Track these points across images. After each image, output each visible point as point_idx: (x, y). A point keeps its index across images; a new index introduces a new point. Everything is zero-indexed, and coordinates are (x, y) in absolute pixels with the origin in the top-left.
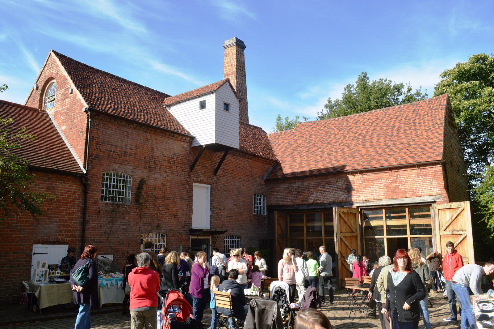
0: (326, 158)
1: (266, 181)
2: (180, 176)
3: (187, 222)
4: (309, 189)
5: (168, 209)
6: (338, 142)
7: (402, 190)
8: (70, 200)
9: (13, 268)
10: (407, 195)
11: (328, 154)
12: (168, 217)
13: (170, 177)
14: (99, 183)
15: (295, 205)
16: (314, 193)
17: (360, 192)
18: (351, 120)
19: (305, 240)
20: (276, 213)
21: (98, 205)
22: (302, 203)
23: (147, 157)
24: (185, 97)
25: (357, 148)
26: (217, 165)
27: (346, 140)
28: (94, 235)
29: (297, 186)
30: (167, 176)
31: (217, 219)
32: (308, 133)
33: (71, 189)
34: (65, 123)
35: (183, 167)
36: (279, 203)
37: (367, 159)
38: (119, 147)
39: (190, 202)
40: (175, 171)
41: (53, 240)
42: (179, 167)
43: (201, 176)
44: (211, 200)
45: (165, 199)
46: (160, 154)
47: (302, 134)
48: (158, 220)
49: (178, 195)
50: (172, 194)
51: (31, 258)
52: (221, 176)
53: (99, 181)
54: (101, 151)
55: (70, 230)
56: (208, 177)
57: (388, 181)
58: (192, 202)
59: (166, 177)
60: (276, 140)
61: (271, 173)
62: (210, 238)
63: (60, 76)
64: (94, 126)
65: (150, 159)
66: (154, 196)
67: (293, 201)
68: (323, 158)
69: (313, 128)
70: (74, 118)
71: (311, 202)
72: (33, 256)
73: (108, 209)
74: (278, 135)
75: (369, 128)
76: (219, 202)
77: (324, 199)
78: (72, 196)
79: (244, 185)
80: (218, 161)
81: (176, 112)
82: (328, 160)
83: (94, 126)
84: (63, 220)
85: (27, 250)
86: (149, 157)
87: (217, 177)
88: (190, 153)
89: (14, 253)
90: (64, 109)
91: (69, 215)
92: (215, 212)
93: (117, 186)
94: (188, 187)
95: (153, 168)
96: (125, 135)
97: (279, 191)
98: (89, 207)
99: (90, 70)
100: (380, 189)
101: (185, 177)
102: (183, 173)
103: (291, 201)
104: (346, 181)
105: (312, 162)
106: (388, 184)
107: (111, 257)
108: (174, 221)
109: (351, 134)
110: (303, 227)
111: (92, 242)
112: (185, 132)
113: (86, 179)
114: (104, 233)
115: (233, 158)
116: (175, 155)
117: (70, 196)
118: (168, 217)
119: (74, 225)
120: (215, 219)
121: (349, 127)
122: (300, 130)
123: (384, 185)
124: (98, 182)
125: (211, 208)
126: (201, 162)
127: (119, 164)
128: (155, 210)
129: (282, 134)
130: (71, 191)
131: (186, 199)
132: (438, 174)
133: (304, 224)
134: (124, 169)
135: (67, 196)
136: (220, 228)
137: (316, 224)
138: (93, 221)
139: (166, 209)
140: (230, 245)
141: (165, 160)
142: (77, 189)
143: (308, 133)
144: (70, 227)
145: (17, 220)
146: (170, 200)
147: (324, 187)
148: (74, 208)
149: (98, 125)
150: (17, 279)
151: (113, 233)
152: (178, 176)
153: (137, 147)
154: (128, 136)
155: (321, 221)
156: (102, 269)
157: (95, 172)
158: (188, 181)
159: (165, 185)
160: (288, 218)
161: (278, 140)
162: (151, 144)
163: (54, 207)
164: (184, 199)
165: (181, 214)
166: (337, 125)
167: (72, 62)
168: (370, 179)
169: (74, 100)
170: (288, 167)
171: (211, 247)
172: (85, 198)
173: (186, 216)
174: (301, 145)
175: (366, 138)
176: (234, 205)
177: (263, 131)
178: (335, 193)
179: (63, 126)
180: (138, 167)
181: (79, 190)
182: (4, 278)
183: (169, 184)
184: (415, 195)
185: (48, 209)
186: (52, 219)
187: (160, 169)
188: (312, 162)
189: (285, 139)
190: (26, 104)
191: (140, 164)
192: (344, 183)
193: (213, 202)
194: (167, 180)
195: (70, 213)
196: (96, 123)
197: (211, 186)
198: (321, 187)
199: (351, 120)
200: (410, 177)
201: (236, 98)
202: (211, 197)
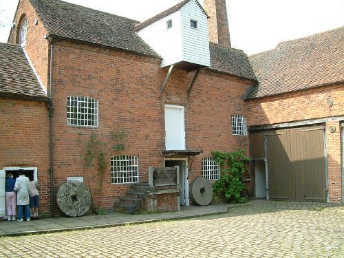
1: (245, 101)
62: (186, 159)
81: (144, 35)
190: (196, 76)
197: (185, 107)
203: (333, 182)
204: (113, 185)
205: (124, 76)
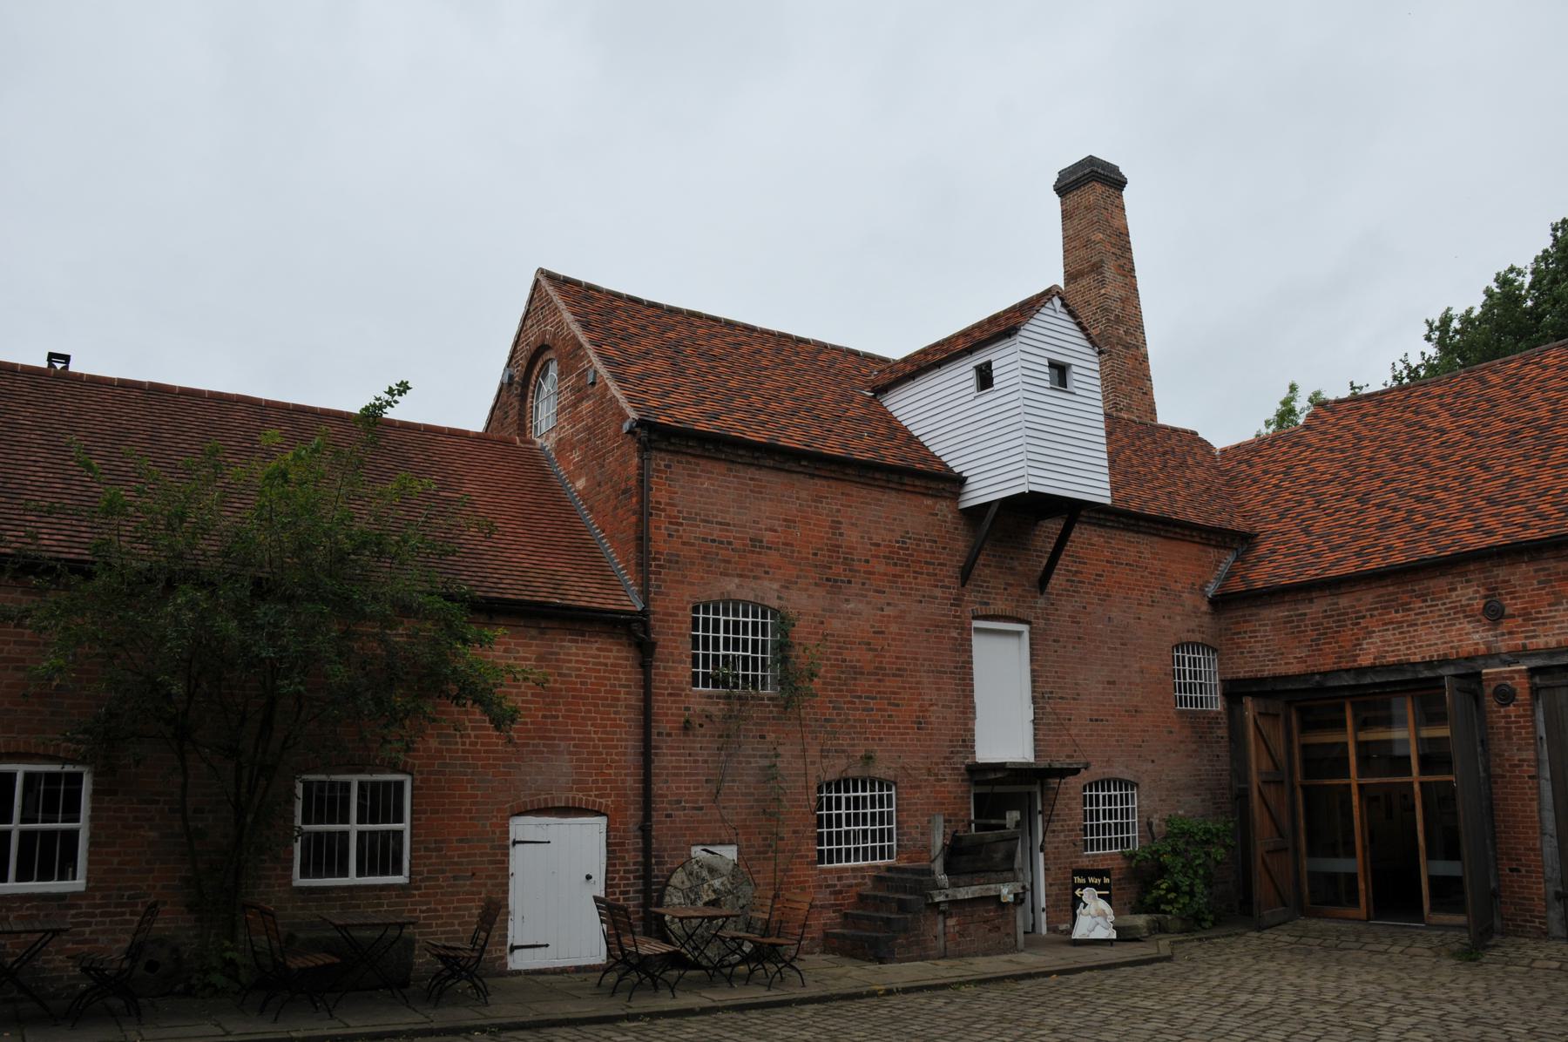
0: (1411, 512)
1: (1214, 602)
2: (930, 602)
4: (1357, 618)
5: (898, 705)
6: (1451, 455)
8: (603, 689)
9: (461, 882)
11: (1418, 499)
12: (899, 728)
13: (896, 605)
14: (684, 635)
15: (1313, 674)
16: (1374, 632)
17: (1537, 619)
18: (1494, 379)
19: (1355, 790)
20: (1248, 702)
21: (684, 702)
22: (1336, 667)
23: (822, 550)
24: (930, 357)
25: (1519, 471)
26: (1045, 562)
27: (1480, 448)
28: (677, 788)
29: (1317, 612)
30: (889, 604)
31: (1055, 730)
32: (1348, 436)
33: (605, 657)
34: (583, 471)
35: (936, 575)
36: (1259, 671)
37: (1553, 504)
39: (964, 679)
40: (911, 589)
41: (563, 805)
42: (922, 573)
43: (994, 599)
44: (1033, 671)
45: (884, 675)
46: (862, 537)
47: (1331, 441)
48: (867, 739)
49: (925, 660)
50: (905, 658)
51: (507, 855)
52: (1061, 595)
53: (683, 631)
54: (684, 543)
55: (610, 775)
56: (1018, 601)
58: (972, 679)
59: (886, 608)
60: (1244, 467)
61: (1231, 574)
63: (564, 339)
64: (659, 471)
65: (829, 556)
66: (852, 667)
67: (1306, 662)
68: (1402, 514)
69: (1364, 416)
70: (604, 455)
71: (1365, 660)
72: (512, 851)
73: (713, 710)
74: (1252, 451)
75: (1559, 400)
76: (1058, 677)
78: (609, 679)
79: (1139, 618)
80: (1049, 548)
82: (1419, 519)
83: (659, 471)
84: (588, 746)
85: (494, 833)
86: (829, 550)
87: (1048, 599)
88: (956, 529)
89: (461, 841)
90: (578, 432)
91: (603, 733)
92: (1049, 710)
93: (736, 641)
94: (955, 635)
95: (842, 581)
96: (751, 491)
97: (1259, 631)
98: (658, 708)
99: (648, 312)
101: (947, 604)
102: (938, 592)
103: (1301, 660)
104: (1483, 584)
105: (1365, 527)
107: (730, 853)
108: (919, 740)
109: (1499, 425)
110: (1346, 744)
111: (672, 810)
112: (937, 466)
113: (646, 627)
114: (707, 781)
115: (1099, 536)
116: (910, 538)
117: (602, 678)
119: (620, 761)
120: (1050, 730)
121: (1488, 401)
122: (1322, 428)
124: (680, 634)
125: (1034, 698)
127: (741, 576)
128: (855, 709)
129: (1265, 446)
130: (606, 665)
131: (951, 673)
133: (1349, 737)
134: (753, 589)
135: (595, 677)
136: (1068, 756)
137: (1398, 734)
138: (672, 748)
139: (889, 704)
140: (1104, 811)
141: (877, 557)
142: (622, 658)
143: (1348, 436)
144: (609, 767)
145: (463, 751)
146: (901, 676)
148: (615, 713)
149: (667, 466)
150: (474, 911)
151: (733, 781)
152: (921, 602)
153: (789, 522)
154: (761, 493)
155: (1404, 723)
156: (705, 886)
158: (955, 616)
159: (883, 632)
161: (1251, 466)
162: (831, 510)
163: (560, 711)
165: (938, 717)
166: (1448, 400)
167: (597, 295)
169: (602, 403)
170: (1285, 551)
171: (1040, 818)
172: (644, 680)
173: (955, 724)
174: (1328, 476)
175: (1549, 434)
176: (1109, 683)
177: (1201, 440)
178: (1445, 626)
179: (579, 479)
180: (796, 583)
181: (627, 659)
182: (440, 907)
183: (894, 628)
185: (544, 717)
186: (559, 745)
187: (863, 584)
188: (1365, 527)
189: (1274, 461)
191: (802, 574)
193: (1038, 676)
194: (889, 616)
195: (605, 726)
196: (662, 463)
197: (1031, 628)
198: (1397, 612)
199: (1494, 379)
201: (1086, 343)
202: (1031, 661)
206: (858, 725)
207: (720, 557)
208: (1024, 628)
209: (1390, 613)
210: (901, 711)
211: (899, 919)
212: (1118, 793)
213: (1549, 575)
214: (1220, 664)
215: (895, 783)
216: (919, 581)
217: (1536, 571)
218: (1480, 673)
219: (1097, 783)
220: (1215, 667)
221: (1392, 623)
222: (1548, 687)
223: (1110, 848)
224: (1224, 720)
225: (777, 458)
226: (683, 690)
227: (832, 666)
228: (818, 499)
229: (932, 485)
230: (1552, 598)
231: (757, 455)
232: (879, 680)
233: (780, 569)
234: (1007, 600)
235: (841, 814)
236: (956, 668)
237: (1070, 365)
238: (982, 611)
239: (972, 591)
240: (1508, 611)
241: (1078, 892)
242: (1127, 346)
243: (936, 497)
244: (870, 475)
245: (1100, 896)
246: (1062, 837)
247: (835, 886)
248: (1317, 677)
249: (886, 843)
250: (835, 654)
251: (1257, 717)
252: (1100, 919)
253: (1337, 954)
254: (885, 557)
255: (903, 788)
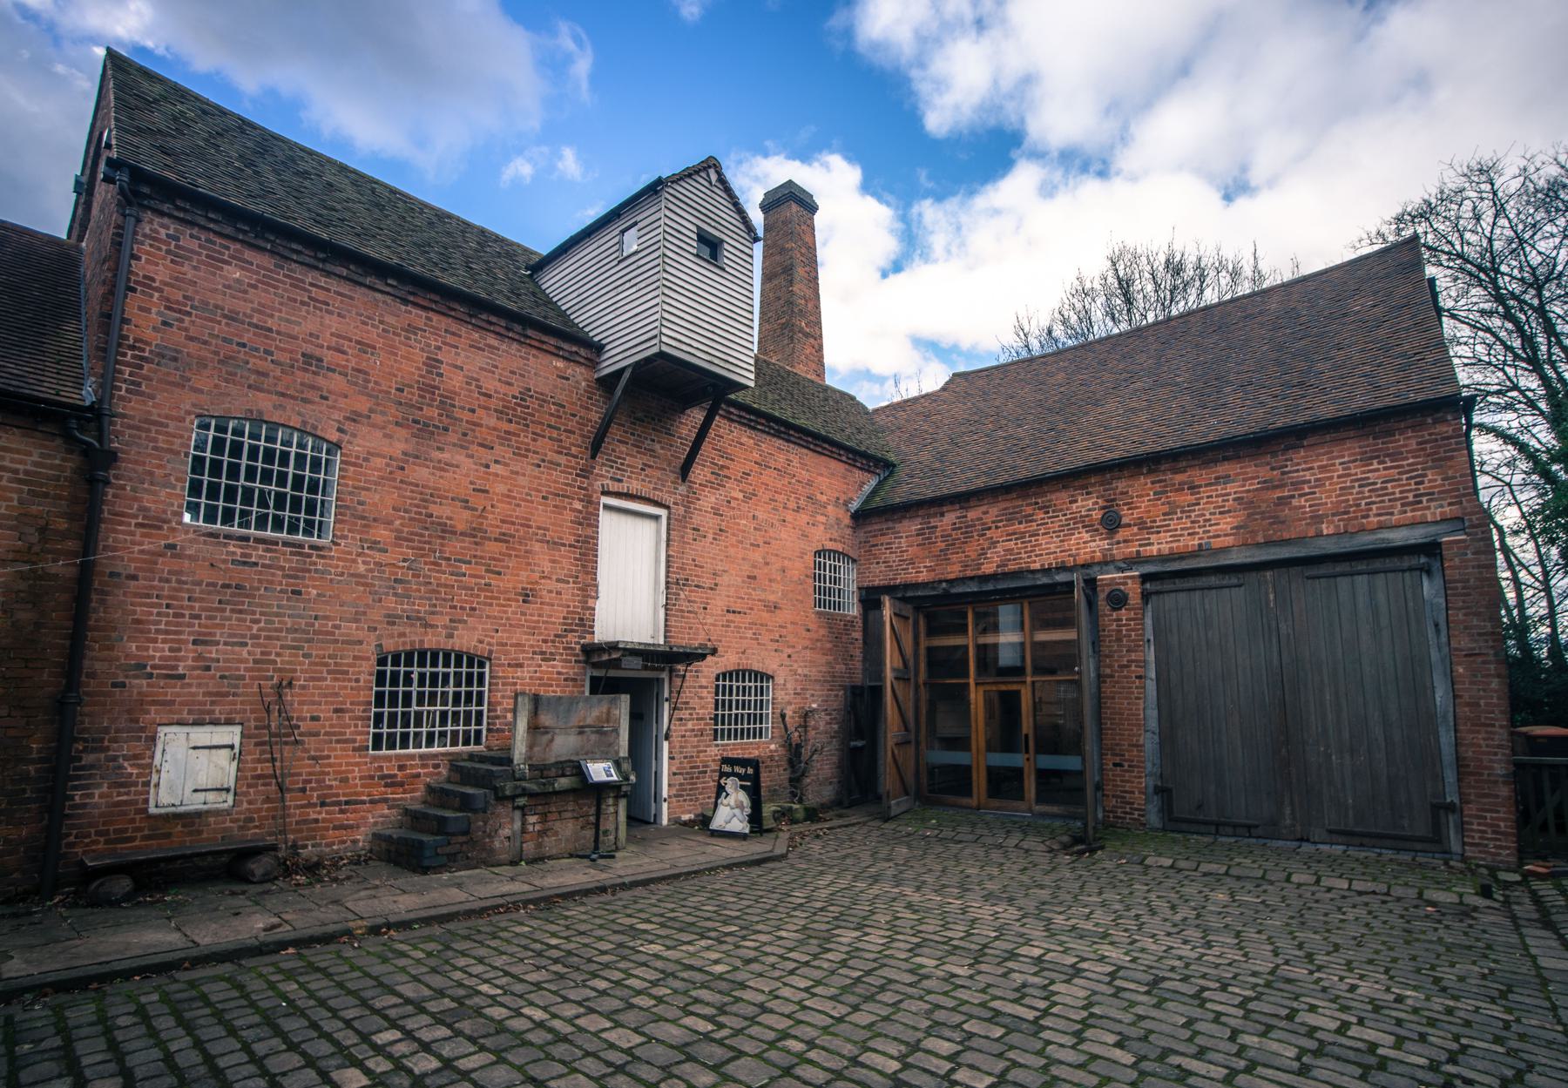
2: (549, 468)
3: (574, 619)
5: (499, 573)
7: (1305, 513)
10: (1324, 526)
15: (940, 582)
17: (1152, 527)
22: (961, 575)
30: (496, 462)
35: (561, 441)
38: (279, 333)
40: (527, 450)
42: (544, 437)
50: (513, 523)
54: (191, 339)
57: (1251, 485)
58: (596, 556)
59: (492, 465)
61: (874, 492)
66: (439, 524)
71: (988, 568)
77: (1029, 557)
81: (554, 282)
87: (690, 487)
92: (682, 596)
100: (1221, 513)
101: (571, 474)
102: (562, 459)
103: (930, 569)
104: (1103, 496)
106: (1250, 494)
110: (966, 647)
116: (531, 397)
118: (498, 598)
123: (1234, 500)
126: (633, 434)
131: (570, 546)
132: (1445, 445)
139: (487, 571)
140: (737, 701)
147: (1031, 521)
152: (539, 466)
157: (154, 410)
158: (580, 488)
160: (922, 622)
164: (564, 545)
168: (1185, 483)
171: (666, 705)
176: (749, 577)
184: (1354, 526)
192: (1097, 503)
196: (163, 232)
198: (1020, 523)
200: (1334, 465)
203: (1117, 760)
204: (375, 758)
205: (455, 381)
206: (443, 590)
207: (249, 366)
208: (663, 513)
209: (1013, 525)
210: (503, 580)
211: (456, 819)
212: (752, 684)
213: (1166, 486)
214: (858, 573)
215: (490, 660)
216: (539, 443)
217: (1153, 483)
218: (1095, 580)
219: (731, 674)
220: (853, 575)
221: (1015, 534)
222: (1158, 593)
223: (742, 738)
224: (859, 624)
225: (352, 267)
226: (168, 521)
227: (411, 519)
228: (412, 329)
229: (566, 346)
230: (1166, 508)
231: (321, 255)
232: (476, 543)
233: (346, 397)
234: (643, 480)
235: (411, 692)
236: (578, 541)
237: (722, 241)
238: (614, 487)
239: (603, 465)
240: (1125, 520)
241: (722, 781)
242: (807, 335)
243: (570, 360)
244: (484, 317)
245: (742, 787)
246: (690, 725)
247: (395, 776)
248: (944, 585)
249: (473, 727)
250: (417, 506)
251: (895, 683)
252: (737, 811)
253: (955, 848)
254: (496, 411)
255: (499, 665)
